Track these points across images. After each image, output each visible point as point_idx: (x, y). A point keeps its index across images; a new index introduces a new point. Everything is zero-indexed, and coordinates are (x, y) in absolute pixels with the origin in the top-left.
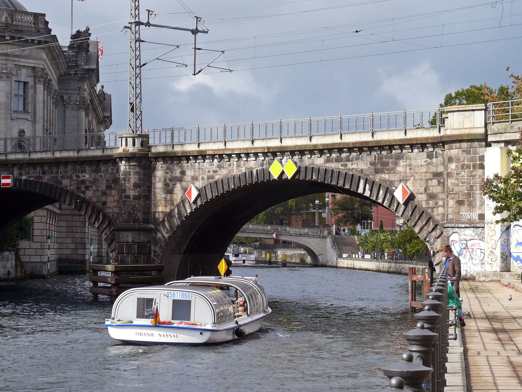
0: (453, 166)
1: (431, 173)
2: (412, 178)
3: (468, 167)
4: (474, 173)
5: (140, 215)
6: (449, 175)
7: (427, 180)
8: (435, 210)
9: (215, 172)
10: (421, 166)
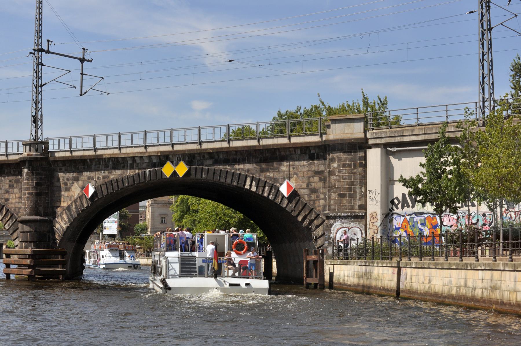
0: (335, 165)
1: (313, 171)
2: (295, 176)
3: (349, 165)
4: (355, 171)
6: (331, 173)
7: (309, 177)
8: (317, 202)
10: (304, 165)
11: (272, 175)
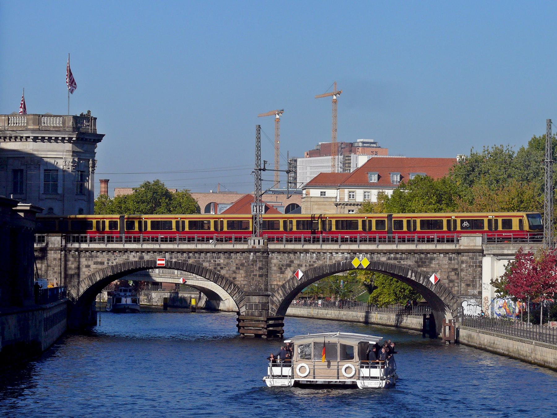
0: (464, 265)
5: (263, 286)
6: (462, 270)
9: (315, 262)
11: (425, 269)
